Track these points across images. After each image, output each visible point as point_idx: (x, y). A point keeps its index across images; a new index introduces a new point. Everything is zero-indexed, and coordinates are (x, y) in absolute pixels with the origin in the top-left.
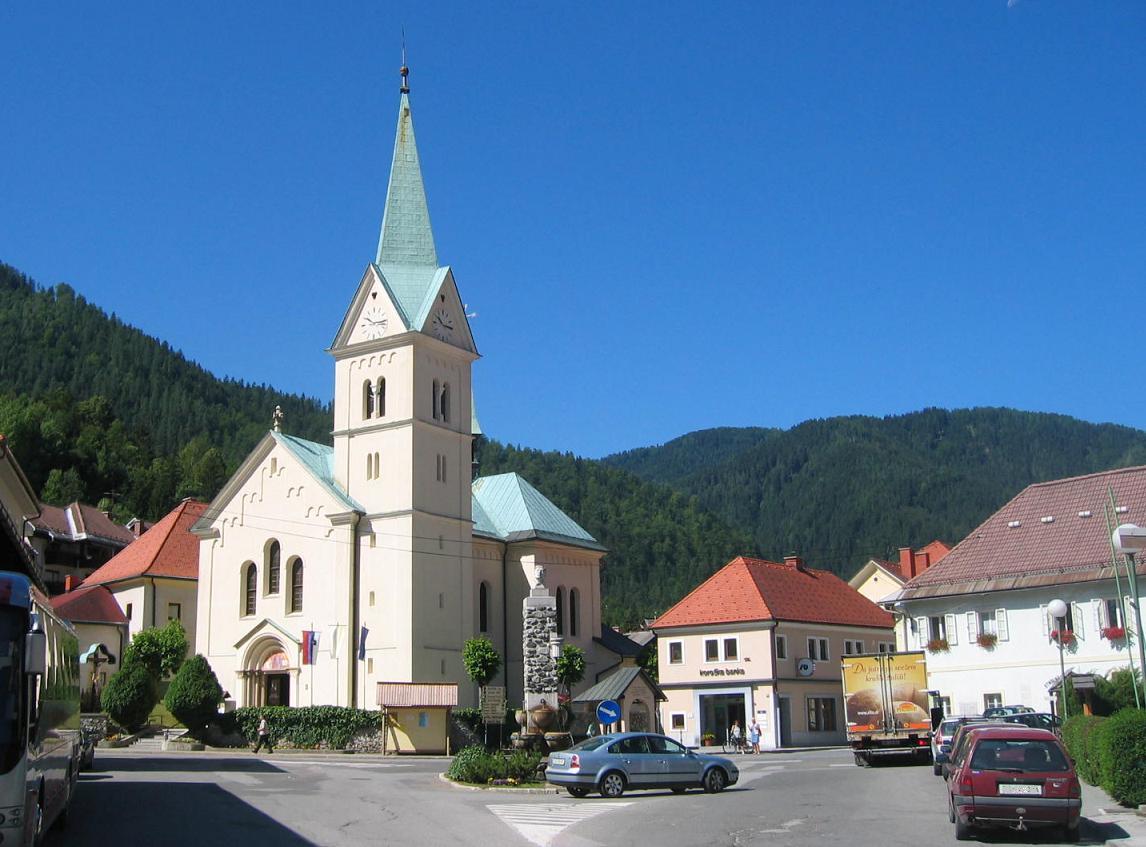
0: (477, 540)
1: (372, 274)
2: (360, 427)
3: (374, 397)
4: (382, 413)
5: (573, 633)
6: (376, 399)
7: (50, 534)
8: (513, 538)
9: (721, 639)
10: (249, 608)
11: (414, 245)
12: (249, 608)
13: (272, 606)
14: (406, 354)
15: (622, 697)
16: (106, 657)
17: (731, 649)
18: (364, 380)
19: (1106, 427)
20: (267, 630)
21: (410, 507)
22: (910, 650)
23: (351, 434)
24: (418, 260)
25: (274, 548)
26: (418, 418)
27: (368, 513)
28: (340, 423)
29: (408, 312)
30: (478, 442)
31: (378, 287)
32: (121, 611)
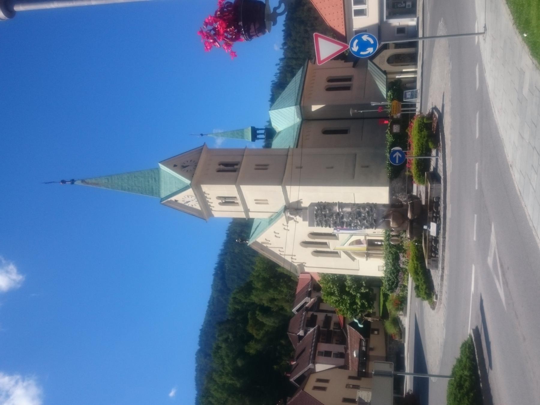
0: (300, 144)
1: (166, 202)
3: (227, 201)
4: (235, 197)
7: (310, 290)
8: (300, 116)
11: (150, 179)
14: (205, 188)
15: (385, 73)
18: (218, 205)
21: (279, 188)
22: (286, 254)
23: (247, 211)
24: (157, 179)
25: (306, 244)
26: (235, 181)
27: (285, 204)
28: (243, 215)
29: (181, 186)
31: (173, 199)
32: (383, 96)
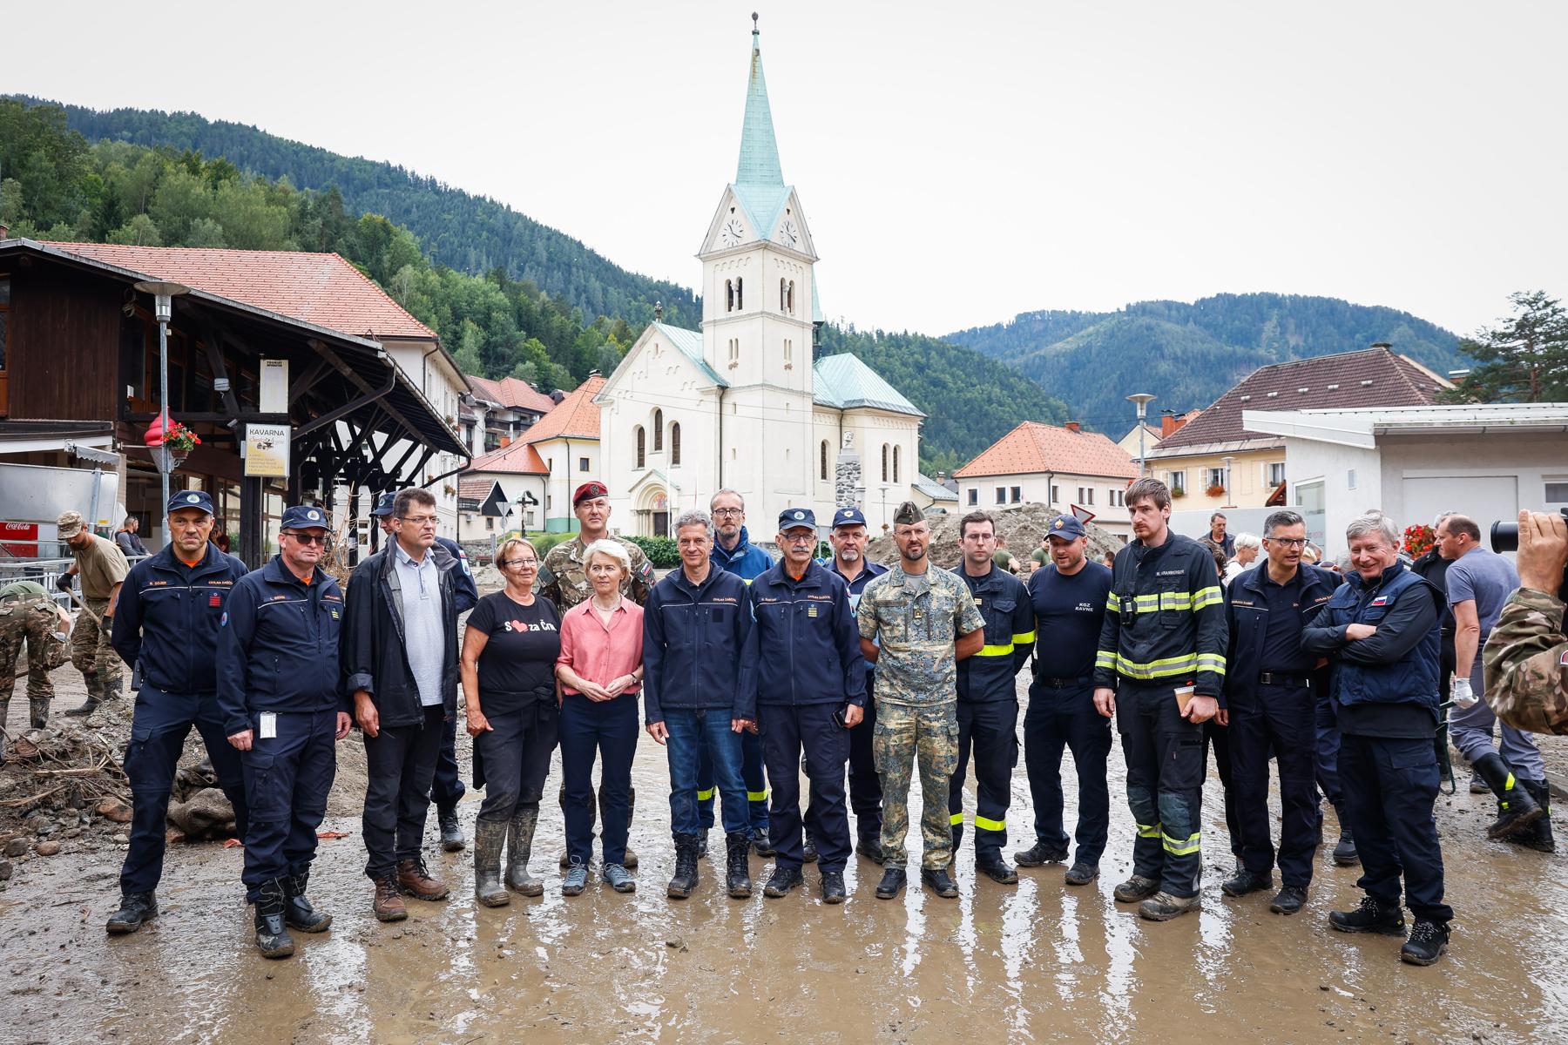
2: (723, 317)
4: (740, 308)
5: (895, 480)
6: (736, 295)
9: (1008, 485)
10: (641, 463)
12: (641, 463)
13: (658, 461)
16: (532, 500)
17: (1016, 493)
19: (1376, 309)
20: (652, 479)
25: (658, 414)
30: (819, 328)
